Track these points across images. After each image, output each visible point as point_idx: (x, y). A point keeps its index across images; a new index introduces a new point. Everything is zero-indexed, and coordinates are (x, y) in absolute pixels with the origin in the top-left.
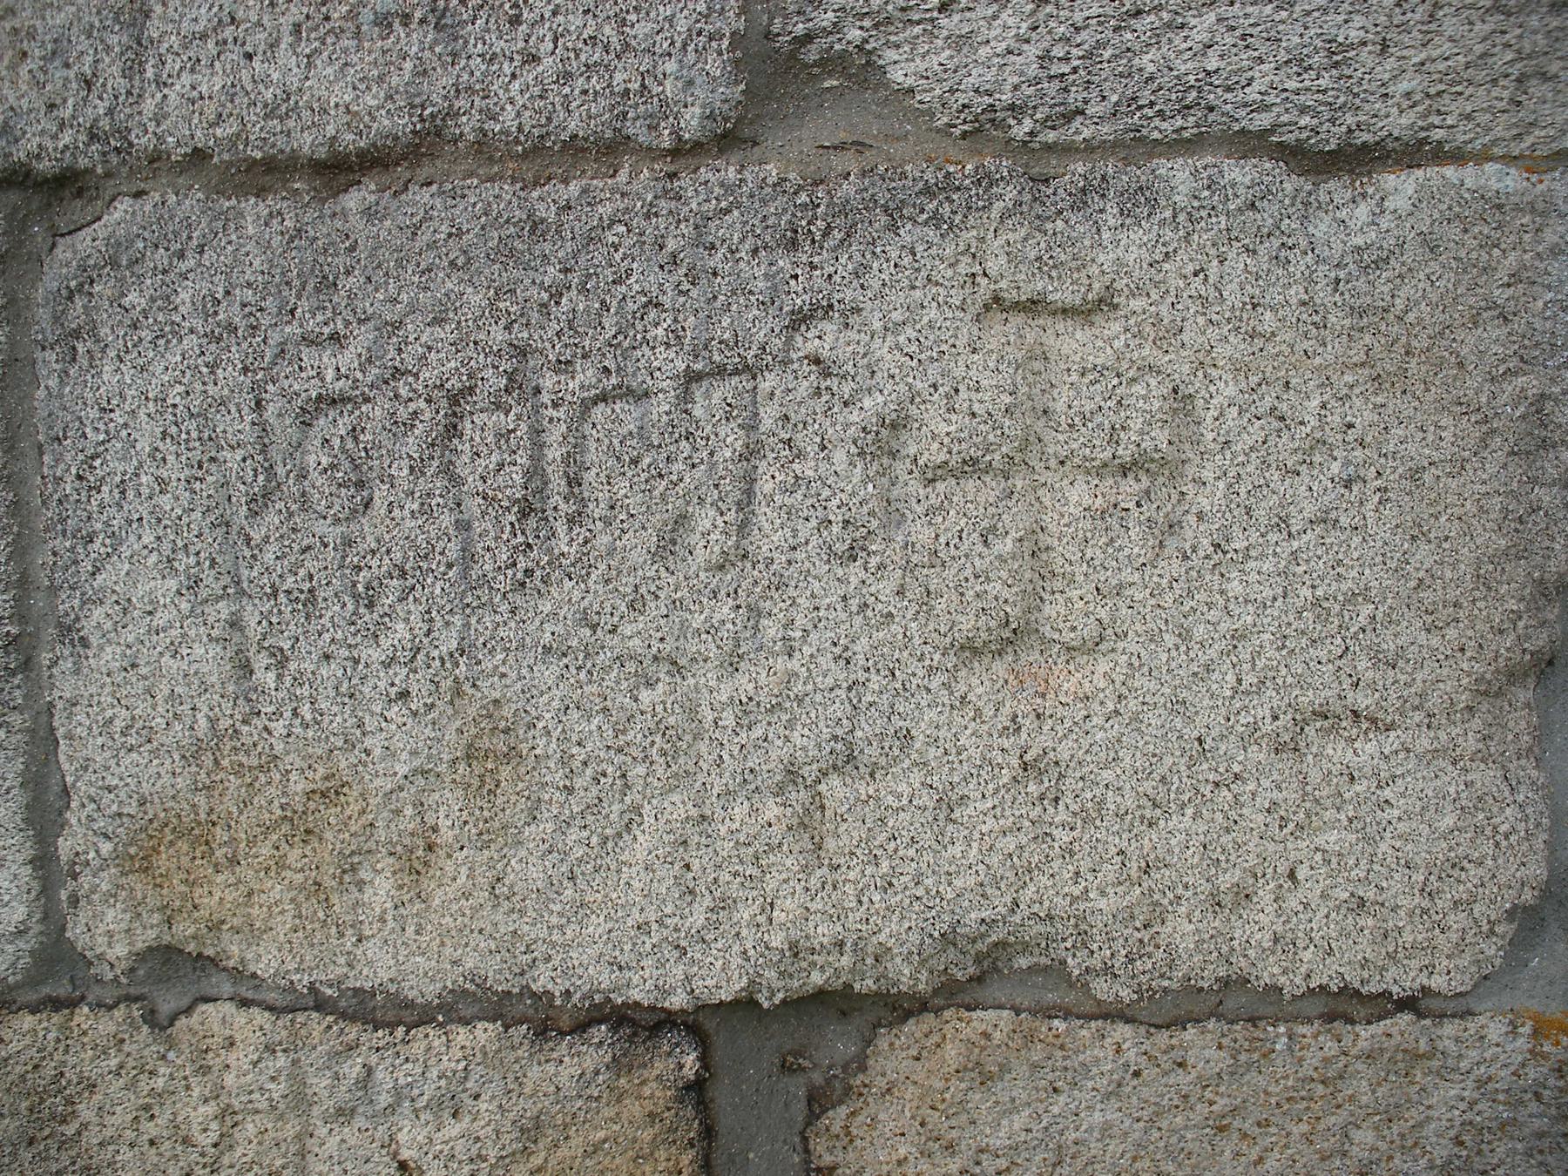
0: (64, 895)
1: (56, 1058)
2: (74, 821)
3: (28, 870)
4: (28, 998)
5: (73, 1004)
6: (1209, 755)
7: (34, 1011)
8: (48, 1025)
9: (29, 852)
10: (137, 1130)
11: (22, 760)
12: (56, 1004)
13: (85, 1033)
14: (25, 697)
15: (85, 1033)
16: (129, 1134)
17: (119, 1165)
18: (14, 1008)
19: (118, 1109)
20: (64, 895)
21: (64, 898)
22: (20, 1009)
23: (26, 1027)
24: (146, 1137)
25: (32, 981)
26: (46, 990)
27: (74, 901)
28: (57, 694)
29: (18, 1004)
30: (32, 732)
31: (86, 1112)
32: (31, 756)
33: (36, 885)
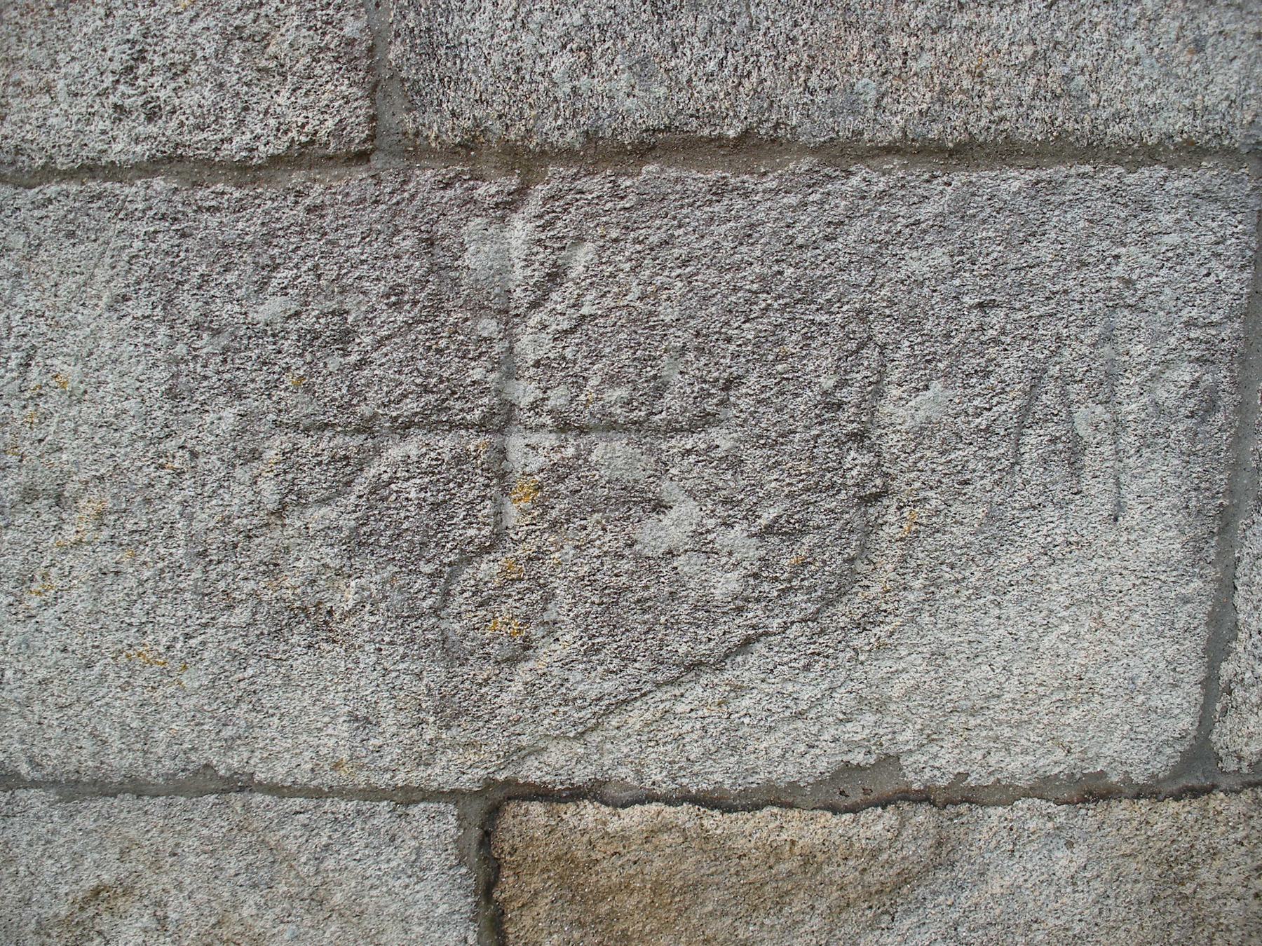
0: (1218, 707)
1: (1191, 833)
2: (1240, 649)
3: (1198, 689)
4: (1170, 789)
5: (1208, 790)
6: (181, 80)
7: (1177, 799)
8: (1186, 810)
9: (1201, 676)
10: (1246, 886)
11: (1210, 603)
12: (1196, 793)
13: (1220, 813)
14: (1218, 554)
15: (1220, 813)
16: (1240, 890)
17: (1223, 915)
18: (1161, 797)
19: (1234, 871)
20: (1218, 707)
21: (1218, 709)
22: (1165, 798)
23: (1171, 811)
24: (1253, 891)
25: (1176, 774)
26: (1183, 782)
27: (1225, 712)
28: (1245, 550)
29: (1163, 794)
30: (1220, 580)
31: (1204, 874)
32: (1218, 600)
33: (1201, 700)
